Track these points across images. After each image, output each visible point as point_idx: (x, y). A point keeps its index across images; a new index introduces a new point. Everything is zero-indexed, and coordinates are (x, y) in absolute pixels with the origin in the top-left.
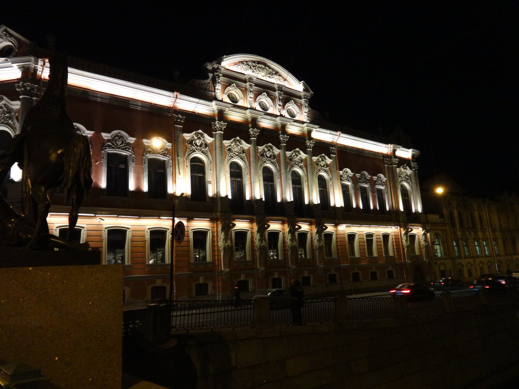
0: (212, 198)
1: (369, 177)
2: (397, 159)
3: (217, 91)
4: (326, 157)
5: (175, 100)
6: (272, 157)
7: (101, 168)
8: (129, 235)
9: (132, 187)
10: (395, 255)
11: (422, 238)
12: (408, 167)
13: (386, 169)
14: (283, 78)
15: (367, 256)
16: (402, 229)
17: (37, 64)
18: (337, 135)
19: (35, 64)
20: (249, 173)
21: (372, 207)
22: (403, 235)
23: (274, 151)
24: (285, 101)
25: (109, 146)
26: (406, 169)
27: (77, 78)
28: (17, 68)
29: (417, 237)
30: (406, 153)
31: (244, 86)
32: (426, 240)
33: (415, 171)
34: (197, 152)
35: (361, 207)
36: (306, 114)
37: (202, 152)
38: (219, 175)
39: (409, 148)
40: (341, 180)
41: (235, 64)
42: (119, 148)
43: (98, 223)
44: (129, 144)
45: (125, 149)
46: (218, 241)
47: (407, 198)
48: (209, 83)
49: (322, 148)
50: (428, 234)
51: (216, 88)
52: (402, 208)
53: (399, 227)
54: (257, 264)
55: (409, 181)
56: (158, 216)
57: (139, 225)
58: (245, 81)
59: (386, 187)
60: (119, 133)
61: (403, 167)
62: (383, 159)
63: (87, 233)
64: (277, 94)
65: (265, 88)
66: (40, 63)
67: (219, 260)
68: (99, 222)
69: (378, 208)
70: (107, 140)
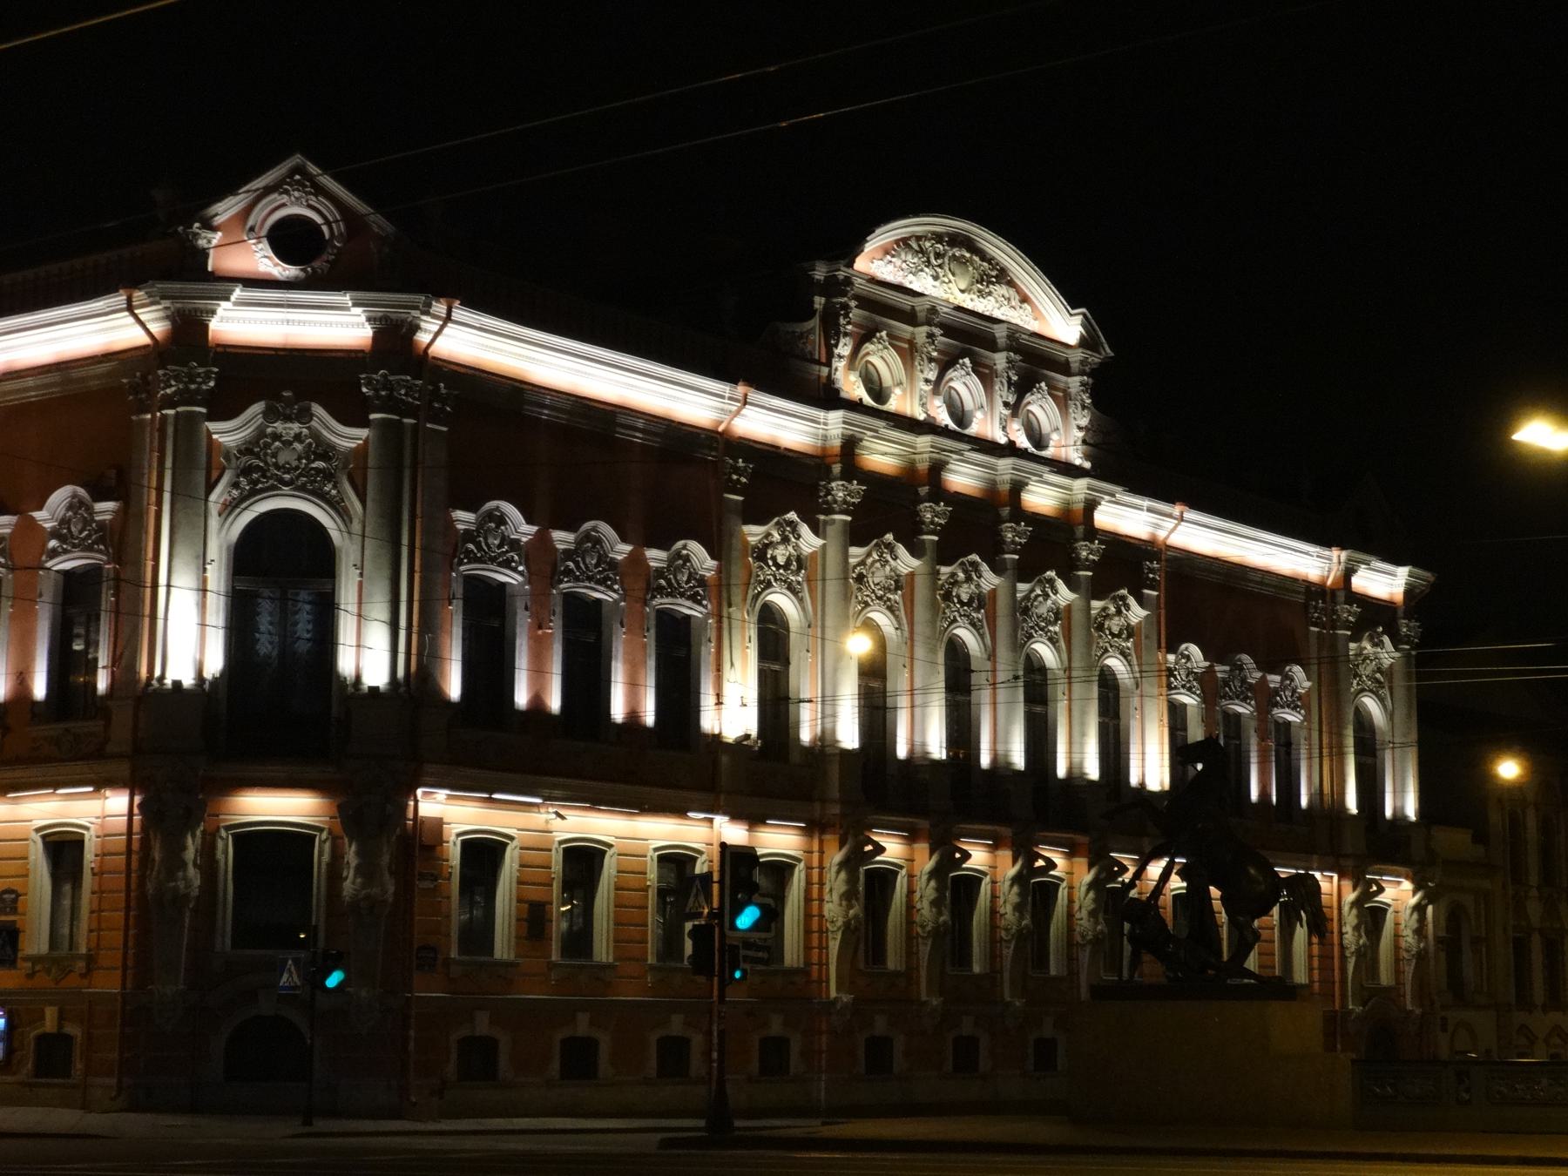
0: (809, 751)
1: (523, 530)
2: (1355, 608)
4: (985, 567)
6: (794, 566)
8: (610, 865)
10: (1399, 982)
11: (1408, 922)
12: (1386, 639)
13: (1313, 641)
14: (1018, 291)
15: (651, 960)
16: (1347, 884)
18: (1170, 516)
20: (907, 662)
21: (1254, 795)
22: (1346, 909)
23: (801, 543)
24: (1023, 387)
26: (1380, 644)
27: (466, 340)
28: (363, 318)
29: (1390, 916)
30: (1384, 582)
31: (908, 336)
32: (1420, 932)
33: (1407, 656)
35: (649, 719)
36: (1081, 434)
39: (1398, 561)
40: (1169, 687)
41: (887, 253)
43: (542, 826)
44: (613, 565)
45: (602, 582)
46: (821, 900)
47: (1370, 761)
48: (813, 329)
49: (1126, 563)
50: (1430, 908)
51: (836, 351)
52: (1352, 803)
53: (1336, 877)
54: (918, 984)
55: (1385, 692)
56: (679, 811)
57: (636, 834)
58: (910, 318)
59: (1307, 718)
61: (1371, 639)
62: (1306, 606)
63: (521, 857)
64: (1000, 360)
65: (967, 340)
67: (824, 964)
68: (547, 822)
69: (1274, 799)
70: (565, 551)
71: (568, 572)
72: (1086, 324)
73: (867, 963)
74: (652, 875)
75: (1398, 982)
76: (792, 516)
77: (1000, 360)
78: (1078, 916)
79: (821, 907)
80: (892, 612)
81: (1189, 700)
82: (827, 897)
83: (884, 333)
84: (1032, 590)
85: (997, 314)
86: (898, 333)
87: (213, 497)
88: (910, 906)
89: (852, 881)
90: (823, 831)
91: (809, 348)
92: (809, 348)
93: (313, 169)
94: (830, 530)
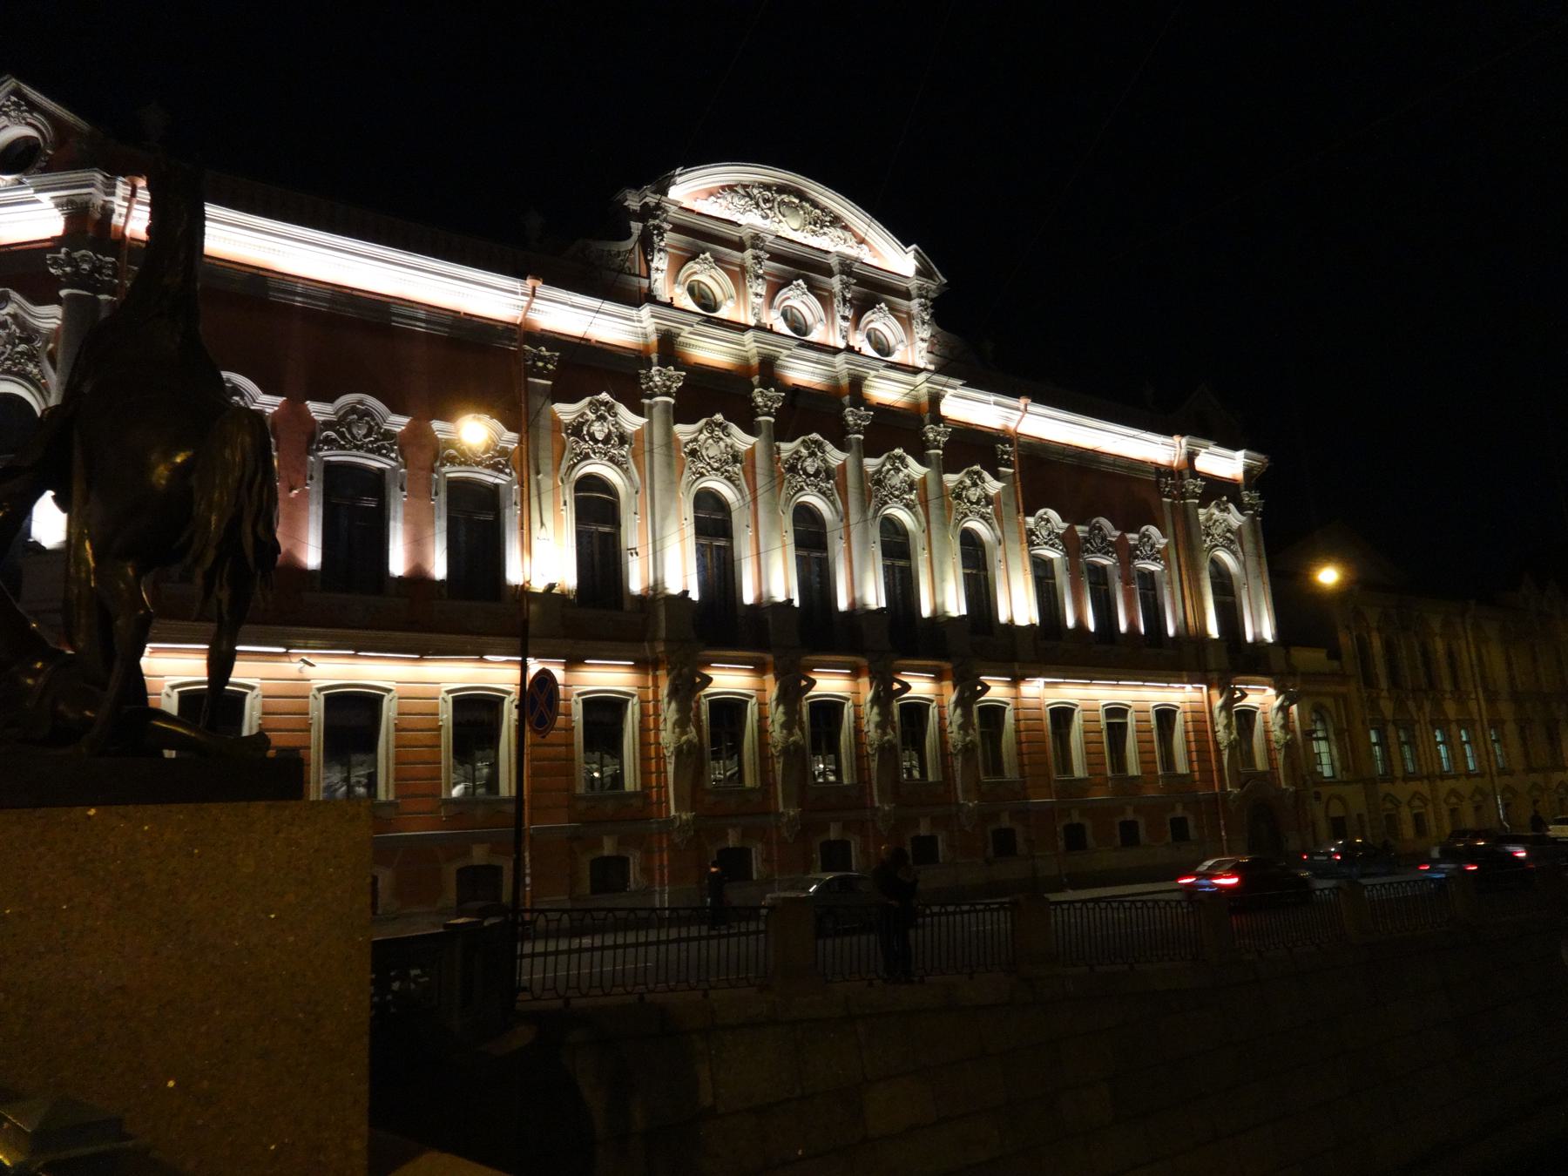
0: (641, 600)
1: (1114, 534)
2: (1199, 482)
3: (654, 275)
4: (986, 475)
5: (530, 303)
6: (822, 475)
7: (306, 509)
8: (389, 710)
9: (398, 564)
10: (1192, 771)
11: (1275, 720)
12: (1231, 506)
13: (1167, 510)
14: (855, 235)
15: (1109, 773)
16: (1215, 693)
17: (113, 194)
18: (1018, 409)
19: (107, 194)
20: (751, 522)
21: (1123, 627)
22: (1216, 712)
23: (828, 457)
24: (861, 306)
25: (329, 442)
26: (1226, 510)
27: (233, 237)
28: (51, 204)
29: (1259, 717)
30: (1225, 464)
31: (738, 261)
32: (1286, 726)
33: (1252, 518)
34: (595, 458)
35: (1092, 626)
36: (925, 345)
37: (611, 459)
38: (662, 528)
39: (1236, 448)
40: (1031, 544)
41: (711, 194)
42: (358, 448)
43: (295, 675)
44: (388, 435)
45: (378, 451)
46: (657, 729)
47: (1229, 599)
48: (631, 251)
49: (973, 447)
50: (1294, 708)
51: (653, 265)
52: (1213, 630)
53: (1205, 687)
54: (776, 799)
55: (1236, 547)
56: (478, 652)
57: (420, 681)
58: (740, 246)
59: (1168, 566)
60: (360, 402)
61: (1218, 506)
62: (1158, 482)
63: (264, 706)
64: (836, 283)
65: (801, 267)
66: (122, 189)
67: (662, 787)
68: (300, 671)
69: (1142, 630)
70: (324, 423)
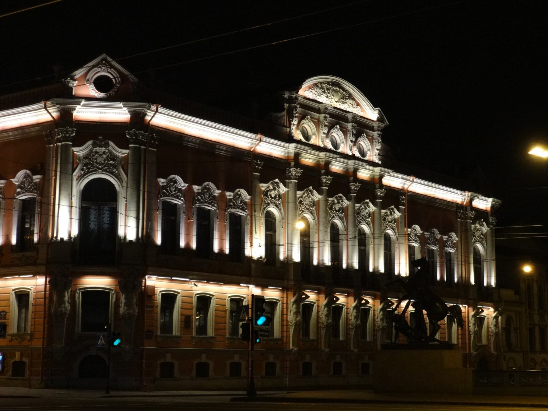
0: (283, 263)
1: (183, 185)
2: (473, 212)
4: (344, 198)
6: (278, 198)
8: (213, 302)
10: (489, 343)
11: (492, 322)
12: (484, 223)
13: (459, 224)
14: (356, 102)
15: (228, 335)
16: (471, 309)
18: (409, 180)
20: (317, 231)
21: (438, 278)
22: (470, 318)
23: (280, 190)
24: (358, 135)
26: (482, 225)
27: (163, 119)
28: (127, 111)
29: (486, 320)
30: (484, 203)
31: (317, 118)
32: (496, 326)
33: (492, 229)
35: (227, 251)
36: (378, 152)
39: (489, 196)
40: (409, 240)
41: (310, 88)
43: (189, 289)
44: (214, 197)
45: (210, 203)
46: (287, 314)
47: (479, 266)
48: (284, 115)
49: (394, 197)
50: (500, 318)
51: (292, 123)
52: (472, 281)
53: (467, 306)
54: (321, 344)
55: (484, 242)
56: (237, 283)
57: (222, 292)
58: (318, 111)
59: (457, 251)
61: (479, 223)
62: (456, 212)
63: (182, 300)
64: (349, 126)
65: (338, 119)
67: (288, 337)
68: (191, 287)
69: (445, 279)
70: (198, 193)
71: (199, 200)
72: (380, 113)
73: (303, 336)
74: (228, 306)
75: (489, 343)
76: (277, 180)
77: (349, 126)
78: (377, 320)
79: (287, 317)
80: (312, 214)
81: (416, 245)
82: (289, 314)
83: (309, 117)
84: (361, 206)
85: (349, 110)
86: (314, 116)
87: (74, 174)
88: (318, 317)
89: (298, 308)
90: (288, 290)
91: (283, 122)
92: (283, 122)
93: (109, 59)
94: (290, 185)
